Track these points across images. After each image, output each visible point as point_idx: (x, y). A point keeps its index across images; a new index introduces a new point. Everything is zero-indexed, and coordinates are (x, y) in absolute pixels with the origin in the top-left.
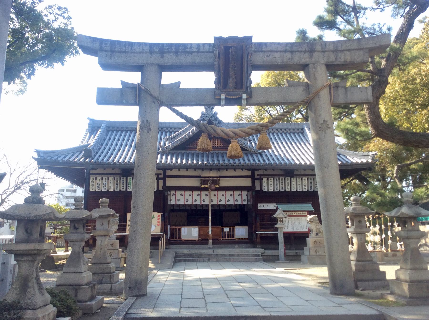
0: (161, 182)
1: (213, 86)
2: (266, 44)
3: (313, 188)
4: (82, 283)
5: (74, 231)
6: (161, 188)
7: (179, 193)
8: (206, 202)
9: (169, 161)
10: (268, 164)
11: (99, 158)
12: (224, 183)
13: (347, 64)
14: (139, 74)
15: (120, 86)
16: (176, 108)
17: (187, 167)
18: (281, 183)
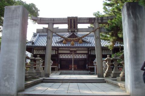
0: (57, 52)
1: (67, 28)
6: (57, 53)
8: (72, 58)
9: (59, 45)
12: (78, 52)
14: (47, 25)
15: (43, 28)
17: (65, 47)
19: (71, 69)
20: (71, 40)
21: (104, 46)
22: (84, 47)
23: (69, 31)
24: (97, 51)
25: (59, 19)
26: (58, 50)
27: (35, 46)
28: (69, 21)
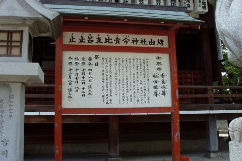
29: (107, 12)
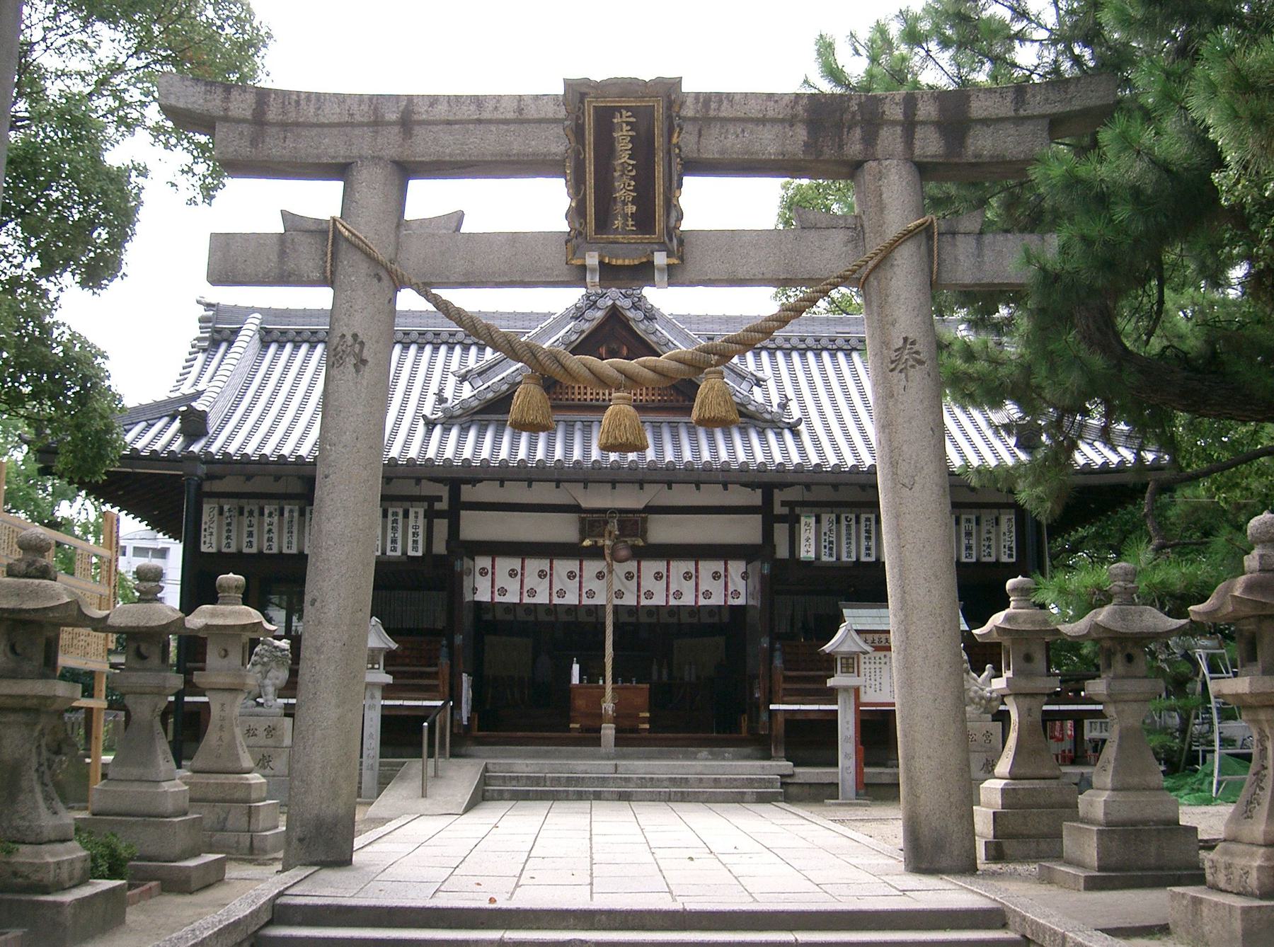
0: (441, 526)
1: (564, 227)
2: (730, 97)
3: (974, 553)
4: (161, 810)
5: (136, 664)
6: (440, 548)
7: (505, 564)
8: (599, 600)
10: (817, 465)
11: (230, 438)
12: (663, 531)
13: (984, 163)
15: (279, 228)
16: (446, 294)
18: (863, 535)
19: (591, 737)
20: (601, 380)
21: (992, 462)
22: (725, 477)
23: (583, 268)
24: (898, 533)
25: (470, 112)
26: (457, 506)
27: (209, 459)
28: (579, 131)
29: (603, 819)
